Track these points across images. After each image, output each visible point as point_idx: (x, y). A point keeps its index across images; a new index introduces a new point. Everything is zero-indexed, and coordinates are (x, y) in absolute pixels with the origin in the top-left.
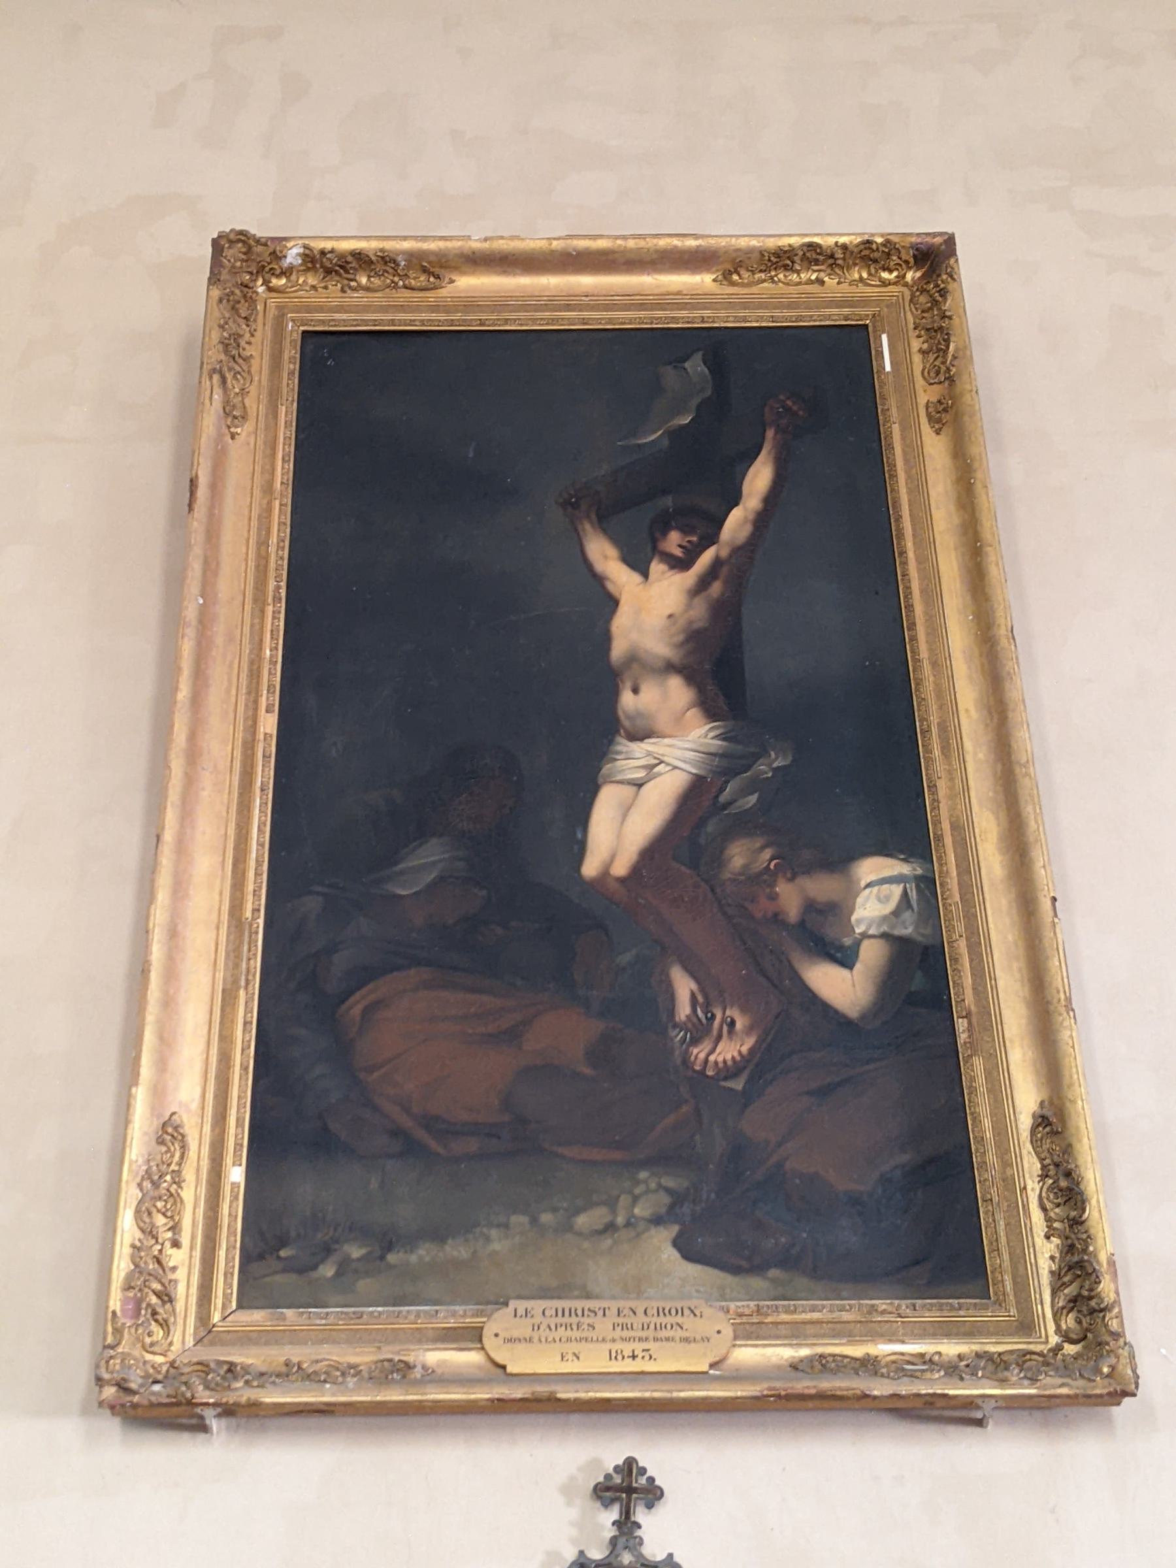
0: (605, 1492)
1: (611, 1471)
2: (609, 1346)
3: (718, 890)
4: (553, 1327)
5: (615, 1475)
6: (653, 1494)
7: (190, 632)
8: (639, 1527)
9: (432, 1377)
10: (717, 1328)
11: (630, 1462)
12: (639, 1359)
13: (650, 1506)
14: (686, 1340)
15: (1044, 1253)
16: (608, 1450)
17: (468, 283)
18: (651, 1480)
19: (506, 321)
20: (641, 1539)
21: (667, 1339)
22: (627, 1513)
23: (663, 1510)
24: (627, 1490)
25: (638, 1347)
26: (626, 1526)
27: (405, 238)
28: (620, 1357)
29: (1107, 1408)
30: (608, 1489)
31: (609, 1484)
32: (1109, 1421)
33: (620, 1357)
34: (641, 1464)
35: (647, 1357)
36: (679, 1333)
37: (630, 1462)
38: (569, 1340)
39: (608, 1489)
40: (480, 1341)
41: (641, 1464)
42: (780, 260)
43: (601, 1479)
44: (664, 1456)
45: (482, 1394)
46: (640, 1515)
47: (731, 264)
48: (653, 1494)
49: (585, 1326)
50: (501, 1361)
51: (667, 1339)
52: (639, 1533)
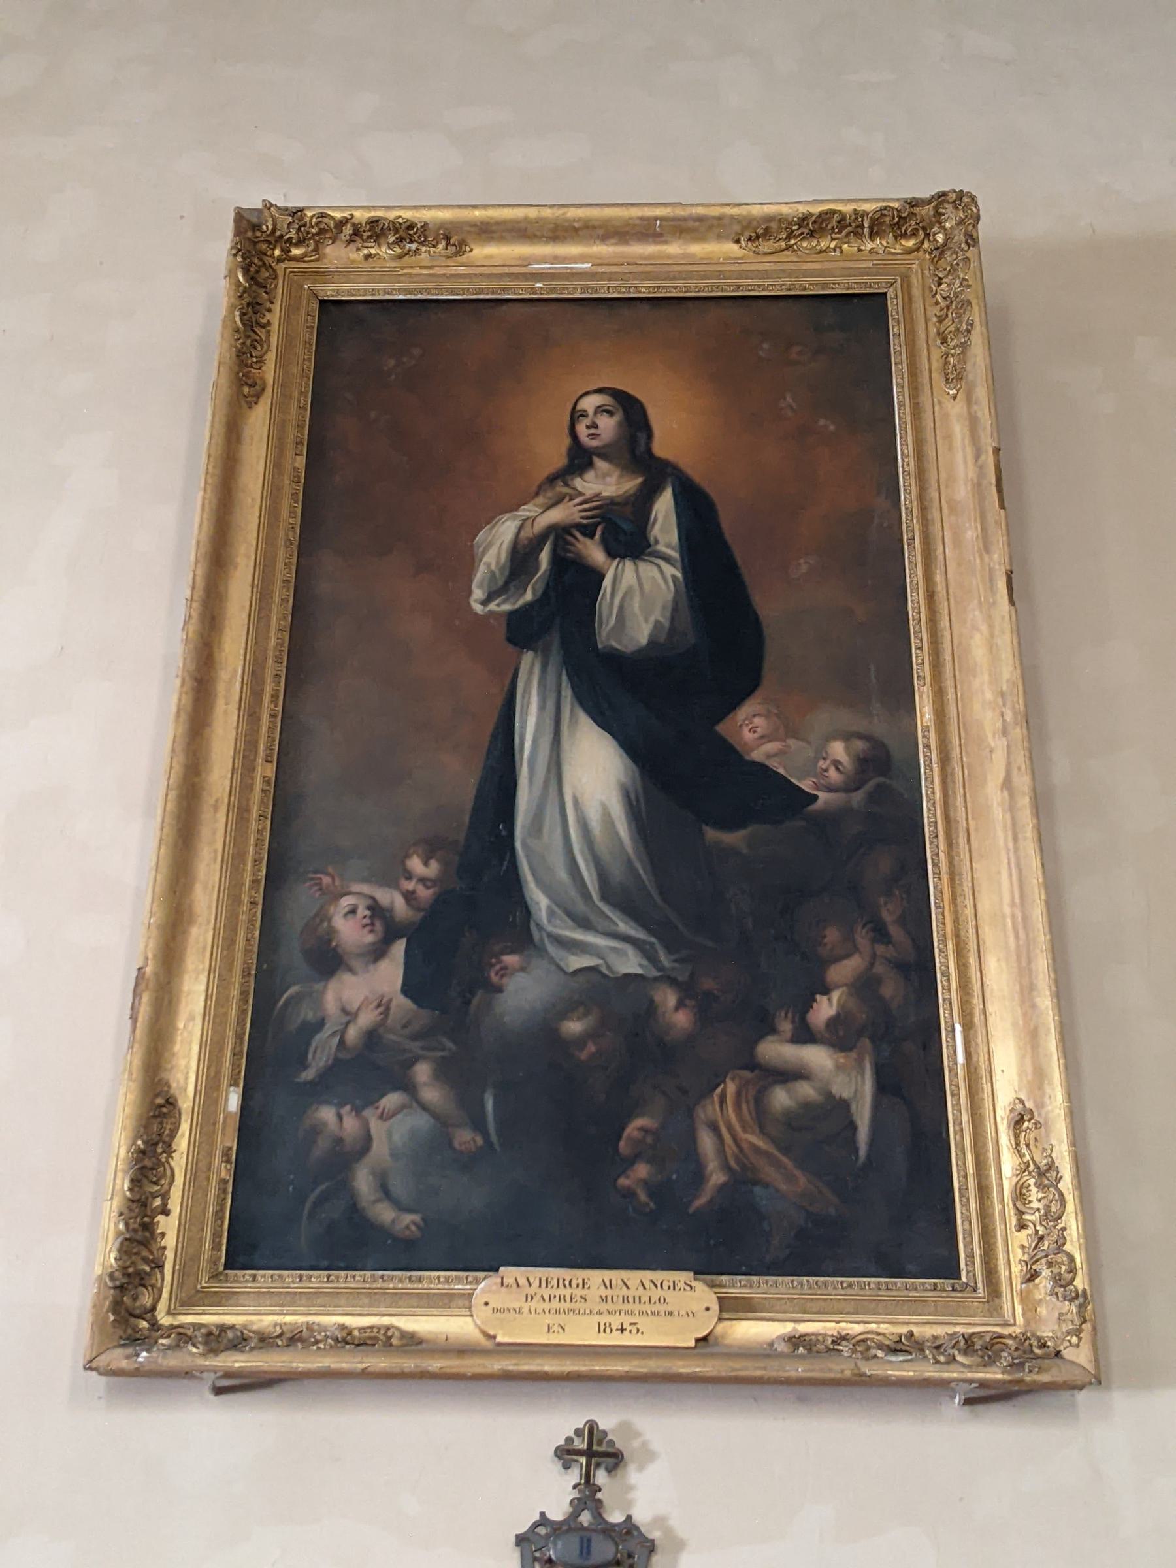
0: (565, 1454)
1: (572, 1434)
2: (597, 1318)
4: (547, 1299)
5: (576, 1439)
6: (613, 1459)
10: (706, 1305)
11: (592, 1426)
12: (626, 1333)
14: (670, 1313)
15: (138, 1025)
17: (484, 252)
19: (504, 290)
21: (653, 1313)
22: (588, 1477)
24: (595, 1454)
25: (627, 1320)
27: (475, 207)
28: (608, 1330)
30: (569, 1452)
31: (570, 1447)
32: (1074, 1405)
33: (608, 1330)
34: (601, 1428)
35: (634, 1331)
36: (662, 1308)
37: (592, 1426)
38: (558, 1312)
39: (569, 1452)
40: (470, 1308)
42: (815, 225)
43: (562, 1442)
47: (758, 231)
48: (613, 1459)
49: (578, 1298)
50: (492, 1333)
51: (653, 1313)
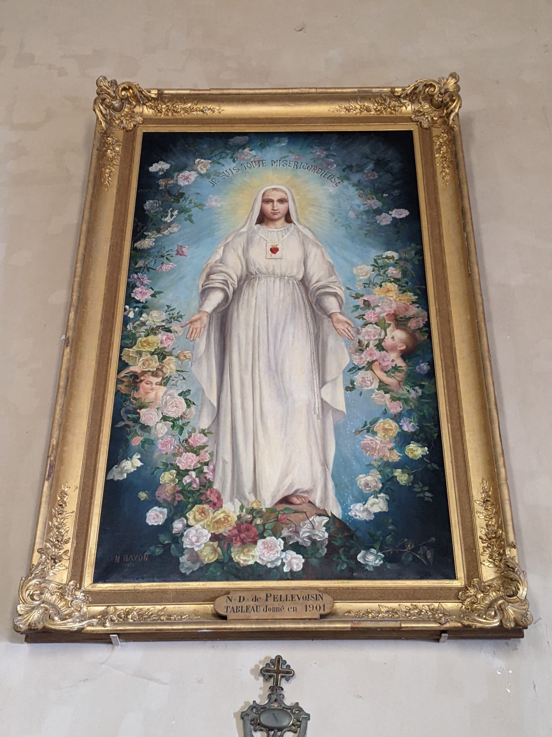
3: (458, 422)
6: (288, 674)
7: (481, 532)
8: (282, 689)
9: (346, 616)
11: (279, 658)
13: (287, 680)
16: (261, 653)
18: (288, 666)
20: (284, 696)
23: (293, 682)
26: (275, 691)
27: (331, 88)
29: (519, 639)
30: (268, 671)
31: (268, 668)
34: (283, 659)
37: (279, 658)
39: (268, 671)
41: (283, 659)
44: (292, 653)
45: (206, 627)
46: (283, 683)
48: (288, 674)
52: (283, 692)
